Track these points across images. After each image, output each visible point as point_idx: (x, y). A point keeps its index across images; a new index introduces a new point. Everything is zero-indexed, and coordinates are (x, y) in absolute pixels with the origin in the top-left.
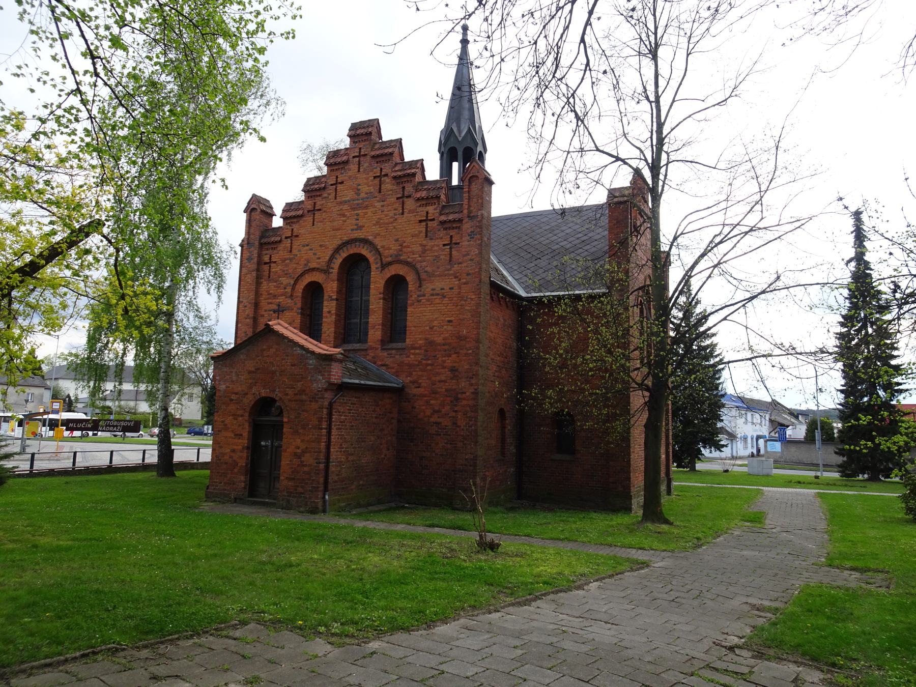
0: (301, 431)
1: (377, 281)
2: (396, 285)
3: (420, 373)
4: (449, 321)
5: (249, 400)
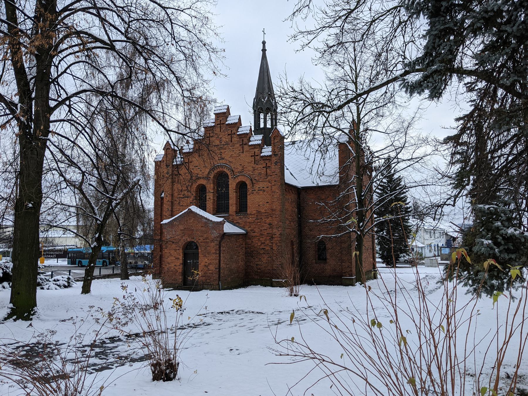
0: (207, 255)
1: (232, 185)
2: (242, 187)
3: (254, 226)
4: (267, 202)
5: (182, 243)
